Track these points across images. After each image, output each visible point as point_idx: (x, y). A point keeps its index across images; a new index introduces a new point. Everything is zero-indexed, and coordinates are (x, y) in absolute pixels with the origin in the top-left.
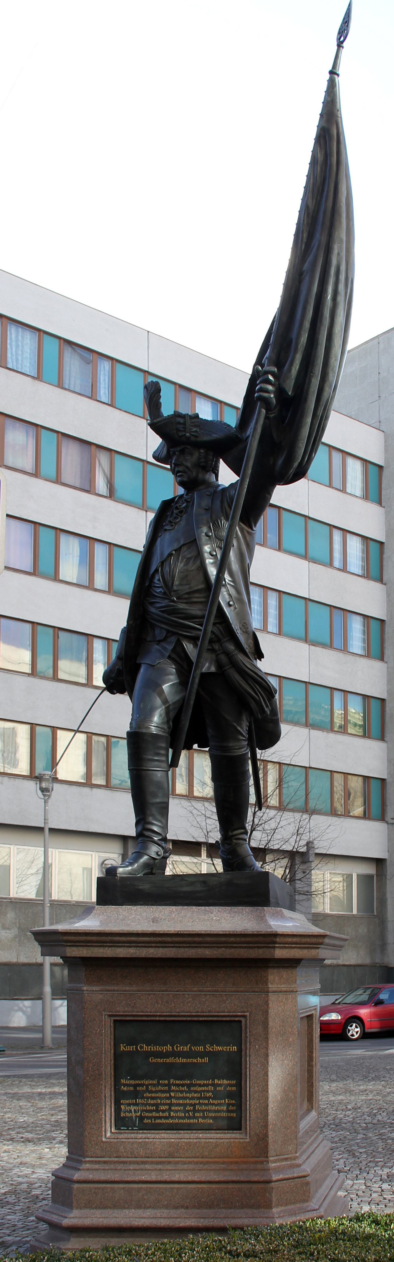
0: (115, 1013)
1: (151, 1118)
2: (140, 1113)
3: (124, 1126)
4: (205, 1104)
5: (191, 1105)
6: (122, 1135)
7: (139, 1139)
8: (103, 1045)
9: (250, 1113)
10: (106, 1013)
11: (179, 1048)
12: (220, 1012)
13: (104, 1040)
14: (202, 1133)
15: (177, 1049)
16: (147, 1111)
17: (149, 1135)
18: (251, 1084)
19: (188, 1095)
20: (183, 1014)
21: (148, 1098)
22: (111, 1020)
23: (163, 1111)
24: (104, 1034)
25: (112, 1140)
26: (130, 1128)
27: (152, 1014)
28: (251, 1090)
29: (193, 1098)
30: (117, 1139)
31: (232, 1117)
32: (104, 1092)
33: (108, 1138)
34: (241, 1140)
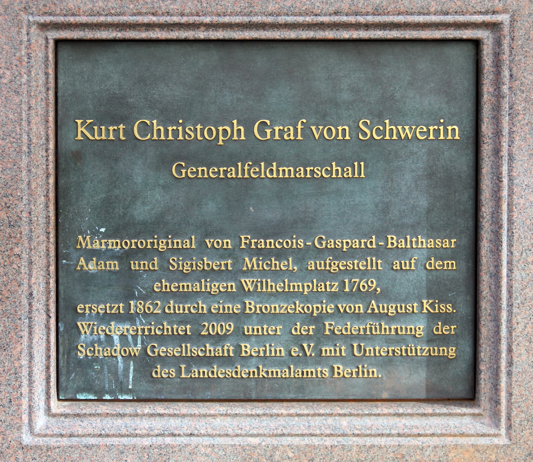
0: (61, 19)
1: (176, 361)
2: (139, 346)
3: (88, 390)
4: (357, 317)
5: (310, 319)
6: (85, 423)
7: (141, 436)
8: (24, 123)
9: (510, 350)
10: (31, 19)
11: (268, 131)
12: (412, 14)
13: (24, 107)
14: (350, 415)
15: (262, 133)
16: (162, 339)
17: (173, 423)
18: (516, 254)
19: (297, 285)
20: (290, 19)
21: (166, 296)
22: (47, 39)
23: (219, 339)
24: (24, 88)
25: (52, 442)
26: (107, 397)
27: (184, 20)
28: (517, 275)
29: (314, 296)
30: (71, 436)
31: (447, 360)
32: (26, 281)
33: (39, 435)
34: (482, 441)
